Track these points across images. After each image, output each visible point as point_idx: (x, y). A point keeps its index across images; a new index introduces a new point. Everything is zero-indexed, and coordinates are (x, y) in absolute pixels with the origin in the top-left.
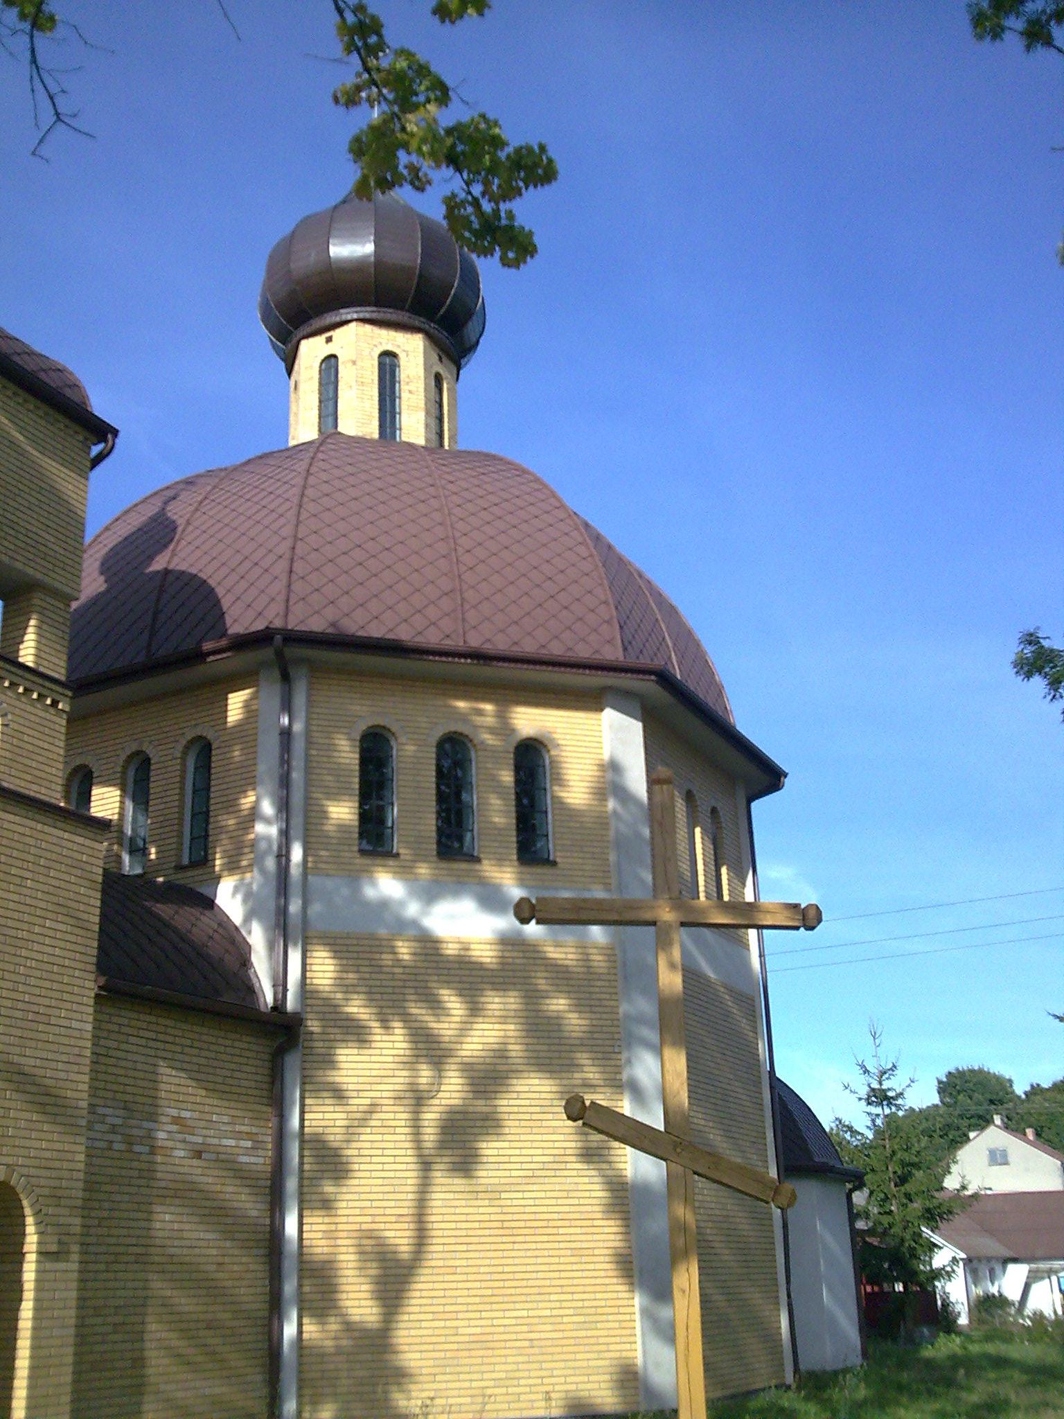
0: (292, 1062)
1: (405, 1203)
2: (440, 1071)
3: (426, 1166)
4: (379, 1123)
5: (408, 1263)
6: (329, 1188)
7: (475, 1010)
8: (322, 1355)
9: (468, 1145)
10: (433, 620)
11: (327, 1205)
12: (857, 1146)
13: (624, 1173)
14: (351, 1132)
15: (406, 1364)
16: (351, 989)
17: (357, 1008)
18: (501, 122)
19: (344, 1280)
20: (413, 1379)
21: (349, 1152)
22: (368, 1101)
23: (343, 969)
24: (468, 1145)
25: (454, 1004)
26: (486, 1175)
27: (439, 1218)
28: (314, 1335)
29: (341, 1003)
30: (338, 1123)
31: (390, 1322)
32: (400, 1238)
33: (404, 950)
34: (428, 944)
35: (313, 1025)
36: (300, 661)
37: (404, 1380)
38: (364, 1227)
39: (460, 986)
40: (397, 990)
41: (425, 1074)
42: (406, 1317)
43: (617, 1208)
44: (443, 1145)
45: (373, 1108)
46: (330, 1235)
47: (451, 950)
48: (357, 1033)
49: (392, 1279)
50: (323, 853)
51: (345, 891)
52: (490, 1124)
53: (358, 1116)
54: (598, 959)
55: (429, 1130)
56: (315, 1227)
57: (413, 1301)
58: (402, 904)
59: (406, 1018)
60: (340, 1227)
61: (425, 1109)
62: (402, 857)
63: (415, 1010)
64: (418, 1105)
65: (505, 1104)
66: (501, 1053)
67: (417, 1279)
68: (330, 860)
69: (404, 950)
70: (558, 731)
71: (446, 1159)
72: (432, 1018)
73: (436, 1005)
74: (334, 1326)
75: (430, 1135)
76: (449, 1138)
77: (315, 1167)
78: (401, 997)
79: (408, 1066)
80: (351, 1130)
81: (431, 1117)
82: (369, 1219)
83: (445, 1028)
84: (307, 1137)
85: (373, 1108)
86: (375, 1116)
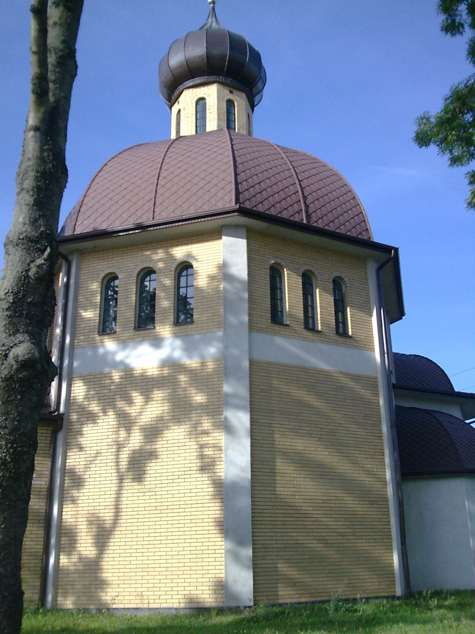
0: (61, 437)
1: (110, 500)
2: (129, 434)
3: (121, 479)
4: (99, 462)
5: (109, 529)
6: (75, 493)
7: (148, 399)
8: (67, 572)
9: (141, 469)
10: (188, 288)
11: (74, 501)
12: (53, 166)
13: (222, 478)
14: (87, 467)
15: (105, 579)
16: (90, 399)
17: (95, 407)
18: (195, 464)
19: (79, 538)
20: (109, 586)
21: (85, 477)
22: (95, 452)
23: (89, 390)
24: (141, 469)
25: (138, 398)
26: (150, 480)
27: (125, 506)
28: (65, 564)
29: (87, 406)
30: (81, 463)
31: (102, 554)
32: (107, 515)
33: (116, 376)
34: (128, 372)
35: (74, 417)
36: (72, 252)
37: (105, 586)
38: (90, 512)
39: (141, 391)
40: (111, 397)
41: (123, 434)
42: (106, 556)
43: (217, 497)
44: (129, 469)
45: (98, 454)
46: (75, 516)
47: (138, 371)
48: (92, 418)
49: (101, 537)
50: (82, 338)
51: (90, 353)
52: (153, 455)
53: (91, 459)
54: (211, 366)
55: (123, 463)
56: (68, 513)
57: (110, 548)
58: (114, 353)
59: (114, 407)
60: (80, 512)
61: (121, 453)
62: (117, 333)
63: (120, 404)
64: (118, 451)
65: (160, 445)
66: (160, 419)
67: (113, 536)
68: (86, 340)
69: (116, 376)
70: (198, 254)
71: (129, 477)
72: (128, 408)
73: (130, 401)
74: (75, 558)
75: (124, 464)
76: (132, 466)
77: (70, 485)
78: (113, 400)
79: (114, 433)
80: (86, 466)
81: (124, 456)
82: (92, 508)
83: (133, 411)
84: (67, 471)
85: (98, 454)
86: (98, 458)
